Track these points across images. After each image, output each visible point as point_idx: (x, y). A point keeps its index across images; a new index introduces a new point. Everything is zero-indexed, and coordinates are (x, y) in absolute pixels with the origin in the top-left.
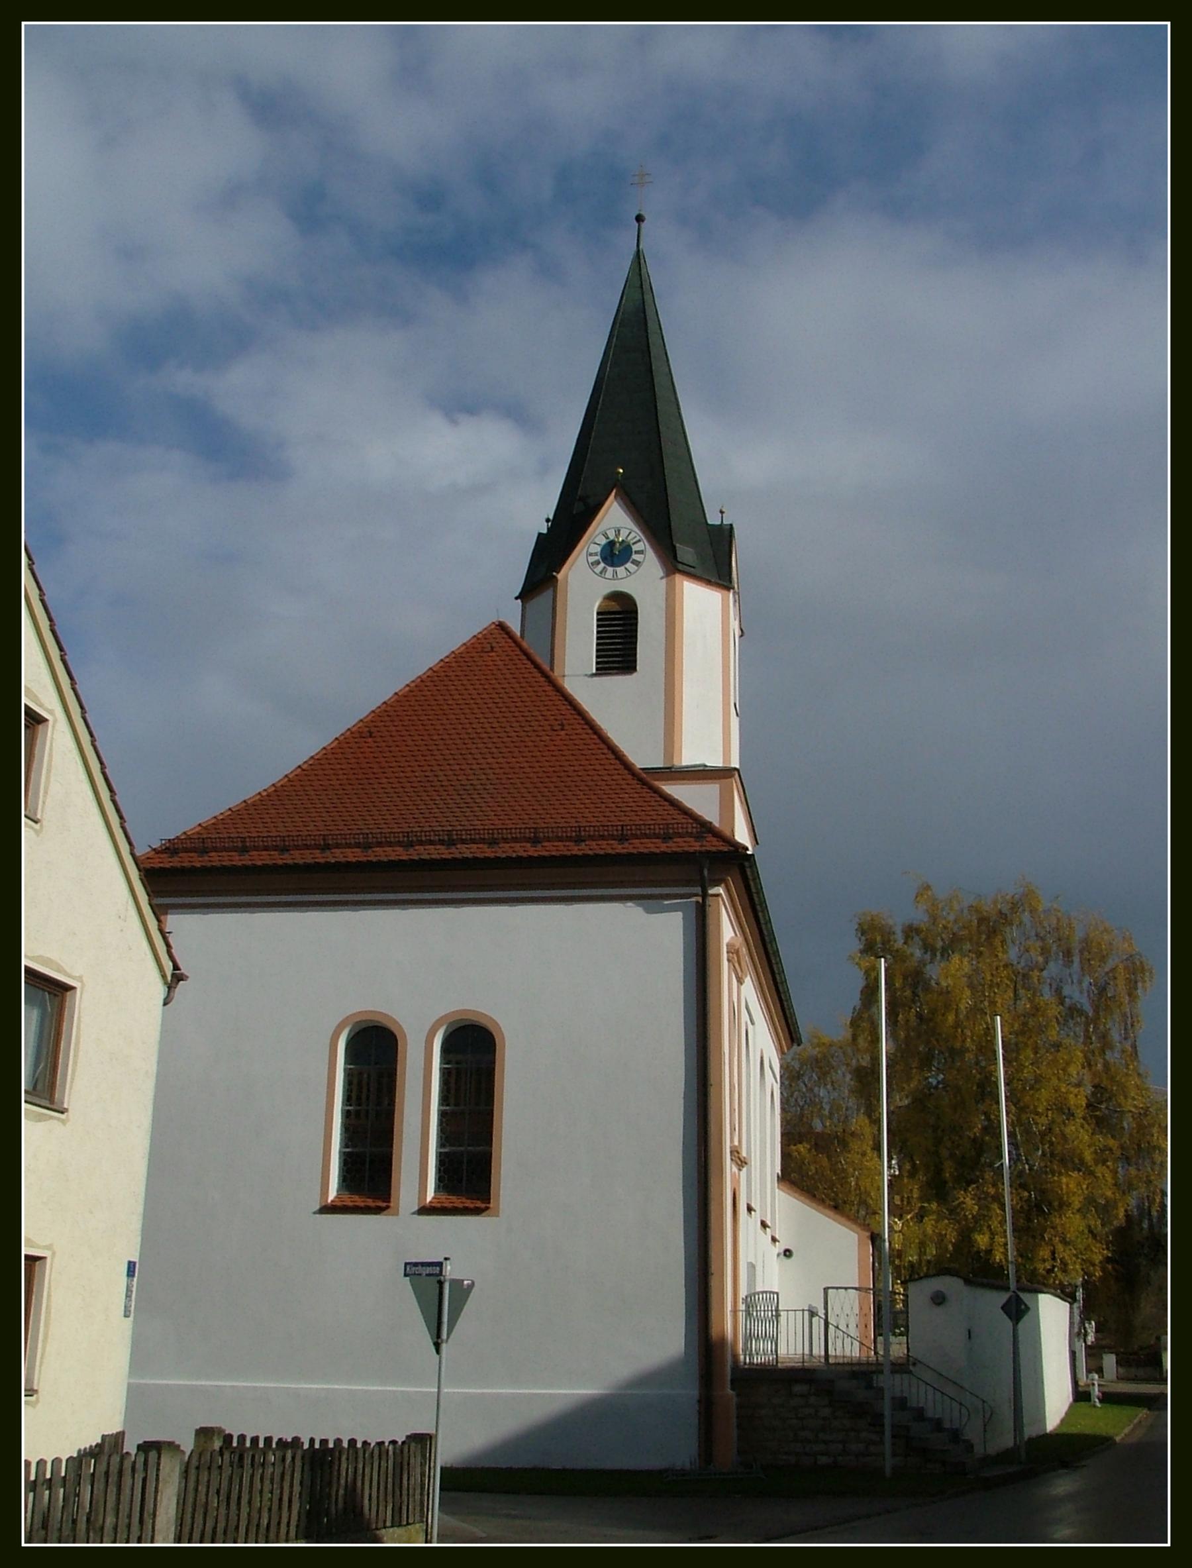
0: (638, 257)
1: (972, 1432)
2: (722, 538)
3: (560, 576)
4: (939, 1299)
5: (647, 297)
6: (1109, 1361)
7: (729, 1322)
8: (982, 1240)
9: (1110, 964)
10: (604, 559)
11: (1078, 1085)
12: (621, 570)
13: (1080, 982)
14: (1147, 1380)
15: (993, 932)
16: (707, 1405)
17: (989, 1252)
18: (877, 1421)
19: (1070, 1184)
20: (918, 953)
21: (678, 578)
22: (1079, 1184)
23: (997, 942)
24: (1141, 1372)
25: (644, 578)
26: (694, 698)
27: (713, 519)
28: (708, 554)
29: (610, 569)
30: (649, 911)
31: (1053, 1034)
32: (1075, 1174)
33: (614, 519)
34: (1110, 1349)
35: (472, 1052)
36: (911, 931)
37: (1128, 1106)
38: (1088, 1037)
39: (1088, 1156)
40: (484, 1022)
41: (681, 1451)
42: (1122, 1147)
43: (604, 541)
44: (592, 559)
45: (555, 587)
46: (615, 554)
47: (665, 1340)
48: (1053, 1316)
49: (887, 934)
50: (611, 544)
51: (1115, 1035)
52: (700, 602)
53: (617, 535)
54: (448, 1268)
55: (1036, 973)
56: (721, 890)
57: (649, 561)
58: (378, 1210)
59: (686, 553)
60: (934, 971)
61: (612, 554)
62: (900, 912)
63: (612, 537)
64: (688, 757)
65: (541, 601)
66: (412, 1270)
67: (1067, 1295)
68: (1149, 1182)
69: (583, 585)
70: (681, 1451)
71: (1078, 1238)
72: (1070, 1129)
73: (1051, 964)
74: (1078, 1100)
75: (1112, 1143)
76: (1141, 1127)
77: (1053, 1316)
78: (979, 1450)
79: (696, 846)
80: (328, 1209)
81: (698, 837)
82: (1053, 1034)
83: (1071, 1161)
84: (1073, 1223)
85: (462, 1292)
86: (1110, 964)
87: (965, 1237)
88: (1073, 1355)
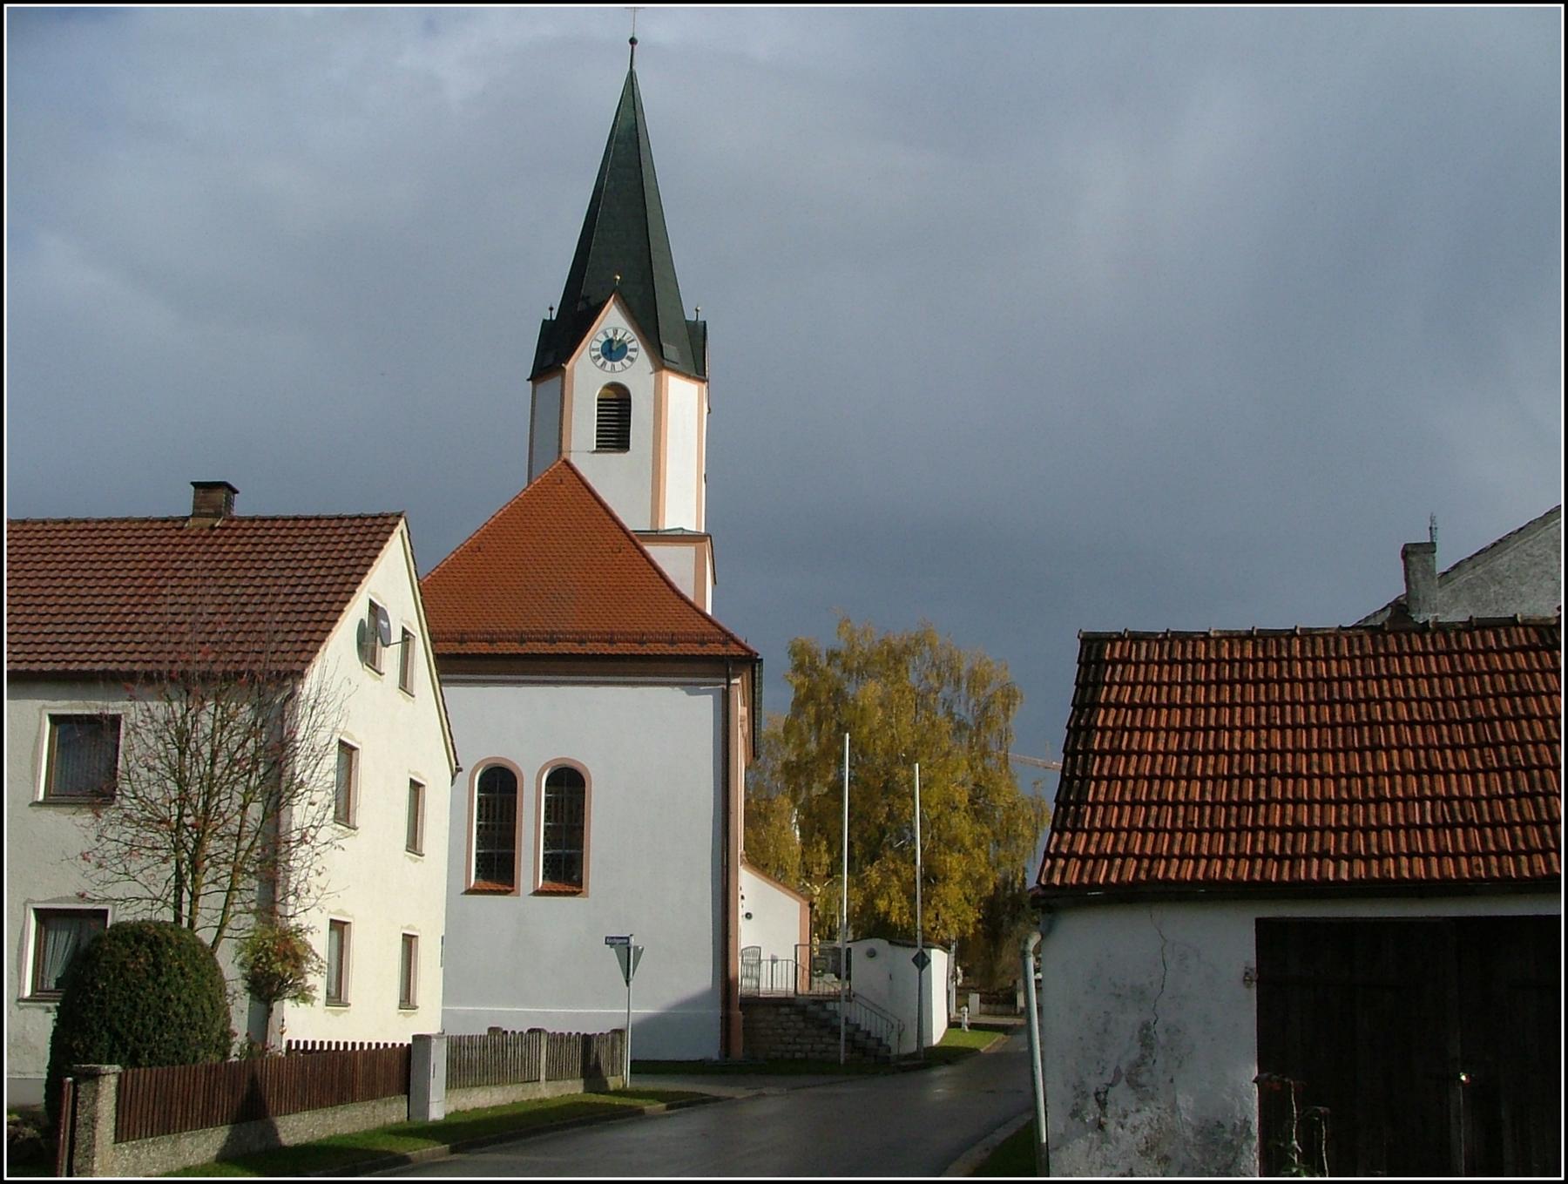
0: (631, 74)
1: (892, 1042)
2: (697, 335)
3: (568, 367)
4: (872, 954)
5: (639, 117)
6: (975, 999)
7: (739, 968)
8: (882, 905)
9: (989, 691)
10: (604, 354)
11: (963, 784)
12: (618, 364)
13: (967, 703)
14: (1007, 1015)
15: (899, 661)
16: (726, 1020)
17: (887, 913)
18: (835, 1031)
19: (953, 862)
20: (839, 673)
21: (664, 373)
22: (960, 863)
23: (902, 668)
24: (999, 1008)
25: (636, 373)
26: (671, 475)
27: (690, 316)
28: (686, 350)
29: (609, 364)
30: (689, 693)
31: (946, 745)
32: (956, 855)
33: (612, 321)
34: (975, 990)
35: (567, 785)
36: (833, 656)
37: (1001, 802)
38: (971, 747)
39: (968, 842)
40: (575, 766)
41: (710, 1049)
42: (994, 833)
43: (604, 339)
44: (595, 354)
45: (563, 377)
46: (613, 350)
47: (699, 978)
48: (939, 961)
49: (814, 657)
50: (610, 341)
51: (993, 747)
52: (684, 399)
53: (616, 333)
54: (632, 940)
55: (932, 696)
56: (738, 681)
57: (641, 357)
58: (506, 893)
59: (670, 350)
60: (850, 689)
61: (611, 351)
62: (824, 639)
63: (611, 335)
64: (670, 522)
65: (553, 383)
66: (610, 941)
67: (945, 946)
68: (1014, 860)
69: (587, 374)
70: (710, 1049)
71: (957, 907)
72: (955, 820)
73: (945, 689)
74: (962, 797)
75: (986, 831)
76: (1009, 818)
77: (939, 961)
78: (894, 1052)
79: (722, 651)
80: (469, 892)
81: (724, 644)
82: (946, 745)
83: (952, 844)
84: (952, 892)
85: (638, 953)
86: (989, 691)
87: (870, 900)
88: (948, 992)
